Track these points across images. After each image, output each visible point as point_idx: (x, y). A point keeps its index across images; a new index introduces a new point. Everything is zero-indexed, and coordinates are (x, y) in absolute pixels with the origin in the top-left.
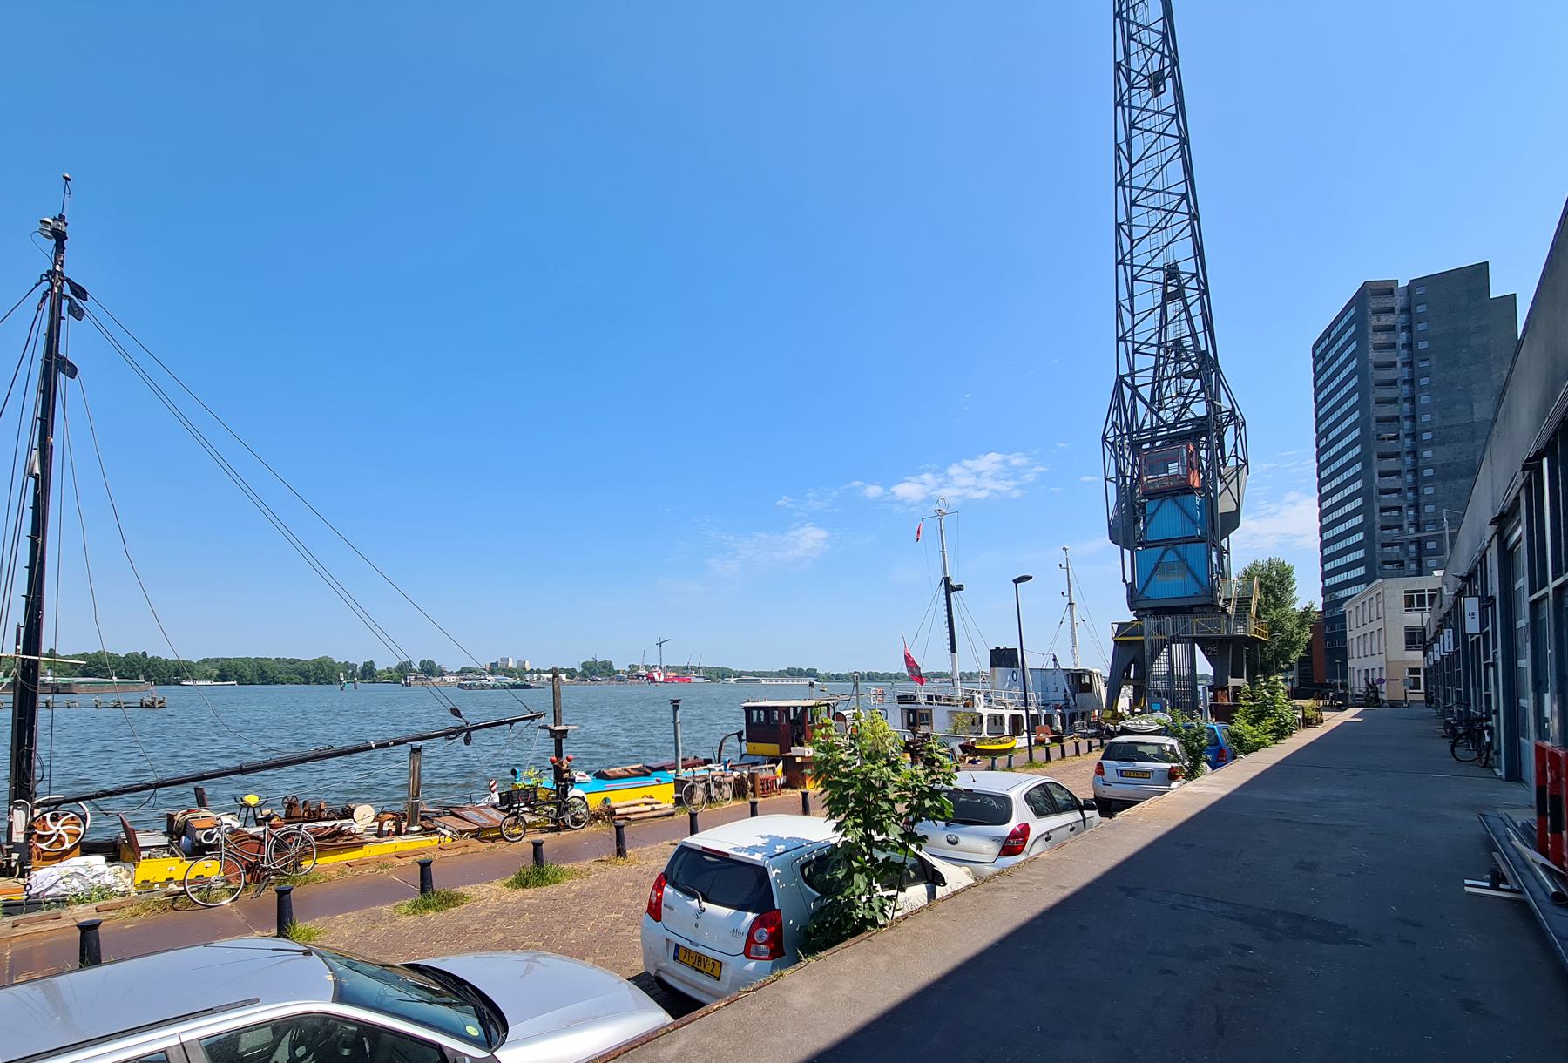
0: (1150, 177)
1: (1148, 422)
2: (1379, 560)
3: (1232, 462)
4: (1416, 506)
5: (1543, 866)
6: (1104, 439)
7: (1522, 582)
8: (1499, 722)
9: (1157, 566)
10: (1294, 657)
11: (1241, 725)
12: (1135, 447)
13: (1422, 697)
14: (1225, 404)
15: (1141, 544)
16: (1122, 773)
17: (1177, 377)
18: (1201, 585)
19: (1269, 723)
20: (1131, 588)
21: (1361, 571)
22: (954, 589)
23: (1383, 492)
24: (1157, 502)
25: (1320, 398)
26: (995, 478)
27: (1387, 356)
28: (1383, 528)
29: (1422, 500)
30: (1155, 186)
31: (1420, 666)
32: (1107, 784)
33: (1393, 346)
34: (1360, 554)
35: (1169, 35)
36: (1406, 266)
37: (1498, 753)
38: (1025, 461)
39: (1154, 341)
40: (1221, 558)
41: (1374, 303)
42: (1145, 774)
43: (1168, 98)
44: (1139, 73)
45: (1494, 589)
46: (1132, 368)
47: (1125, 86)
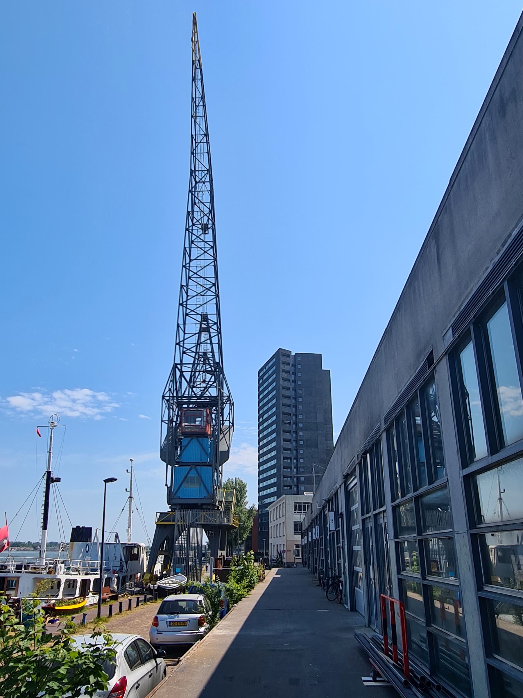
0: (199, 268)
1: (187, 392)
2: (282, 484)
3: (227, 424)
4: (297, 459)
5: (393, 665)
6: (163, 397)
7: (356, 506)
8: (346, 578)
9: (186, 477)
10: (245, 536)
11: (232, 584)
12: (179, 405)
13: (301, 561)
14: (225, 392)
15: (177, 463)
16: (170, 624)
17: (204, 372)
18: (208, 492)
19: (246, 581)
20: (169, 489)
21: (274, 489)
22: (53, 481)
23: (285, 449)
24: (190, 438)
25: (261, 397)
26: (85, 405)
27: (286, 384)
28: (284, 468)
29: (299, 456)
30: (201, 273)
31: (300, 543)
32: (160, 633)
33: (289, 380)
34: (274, 480)
35: (212, 211)
36: (296, 347)
37: (345, 596)
38: (107, 398)
39: (194, 349)
40: (218, 476)
41: (283, 358)
42: (184, 623)
43: (209, 237)
44: (198, 221)
45: (342, 508)
46: (181, 361)
47: (191, 224)
